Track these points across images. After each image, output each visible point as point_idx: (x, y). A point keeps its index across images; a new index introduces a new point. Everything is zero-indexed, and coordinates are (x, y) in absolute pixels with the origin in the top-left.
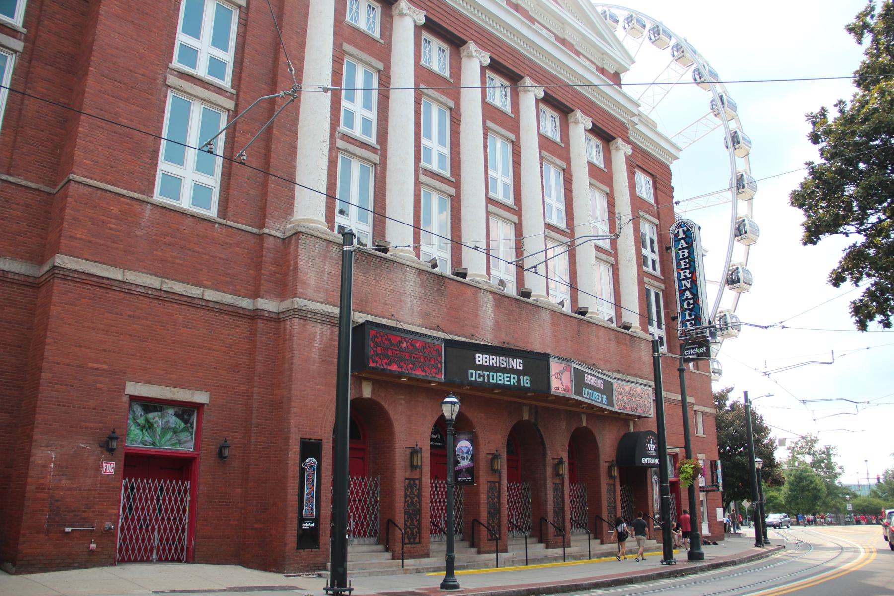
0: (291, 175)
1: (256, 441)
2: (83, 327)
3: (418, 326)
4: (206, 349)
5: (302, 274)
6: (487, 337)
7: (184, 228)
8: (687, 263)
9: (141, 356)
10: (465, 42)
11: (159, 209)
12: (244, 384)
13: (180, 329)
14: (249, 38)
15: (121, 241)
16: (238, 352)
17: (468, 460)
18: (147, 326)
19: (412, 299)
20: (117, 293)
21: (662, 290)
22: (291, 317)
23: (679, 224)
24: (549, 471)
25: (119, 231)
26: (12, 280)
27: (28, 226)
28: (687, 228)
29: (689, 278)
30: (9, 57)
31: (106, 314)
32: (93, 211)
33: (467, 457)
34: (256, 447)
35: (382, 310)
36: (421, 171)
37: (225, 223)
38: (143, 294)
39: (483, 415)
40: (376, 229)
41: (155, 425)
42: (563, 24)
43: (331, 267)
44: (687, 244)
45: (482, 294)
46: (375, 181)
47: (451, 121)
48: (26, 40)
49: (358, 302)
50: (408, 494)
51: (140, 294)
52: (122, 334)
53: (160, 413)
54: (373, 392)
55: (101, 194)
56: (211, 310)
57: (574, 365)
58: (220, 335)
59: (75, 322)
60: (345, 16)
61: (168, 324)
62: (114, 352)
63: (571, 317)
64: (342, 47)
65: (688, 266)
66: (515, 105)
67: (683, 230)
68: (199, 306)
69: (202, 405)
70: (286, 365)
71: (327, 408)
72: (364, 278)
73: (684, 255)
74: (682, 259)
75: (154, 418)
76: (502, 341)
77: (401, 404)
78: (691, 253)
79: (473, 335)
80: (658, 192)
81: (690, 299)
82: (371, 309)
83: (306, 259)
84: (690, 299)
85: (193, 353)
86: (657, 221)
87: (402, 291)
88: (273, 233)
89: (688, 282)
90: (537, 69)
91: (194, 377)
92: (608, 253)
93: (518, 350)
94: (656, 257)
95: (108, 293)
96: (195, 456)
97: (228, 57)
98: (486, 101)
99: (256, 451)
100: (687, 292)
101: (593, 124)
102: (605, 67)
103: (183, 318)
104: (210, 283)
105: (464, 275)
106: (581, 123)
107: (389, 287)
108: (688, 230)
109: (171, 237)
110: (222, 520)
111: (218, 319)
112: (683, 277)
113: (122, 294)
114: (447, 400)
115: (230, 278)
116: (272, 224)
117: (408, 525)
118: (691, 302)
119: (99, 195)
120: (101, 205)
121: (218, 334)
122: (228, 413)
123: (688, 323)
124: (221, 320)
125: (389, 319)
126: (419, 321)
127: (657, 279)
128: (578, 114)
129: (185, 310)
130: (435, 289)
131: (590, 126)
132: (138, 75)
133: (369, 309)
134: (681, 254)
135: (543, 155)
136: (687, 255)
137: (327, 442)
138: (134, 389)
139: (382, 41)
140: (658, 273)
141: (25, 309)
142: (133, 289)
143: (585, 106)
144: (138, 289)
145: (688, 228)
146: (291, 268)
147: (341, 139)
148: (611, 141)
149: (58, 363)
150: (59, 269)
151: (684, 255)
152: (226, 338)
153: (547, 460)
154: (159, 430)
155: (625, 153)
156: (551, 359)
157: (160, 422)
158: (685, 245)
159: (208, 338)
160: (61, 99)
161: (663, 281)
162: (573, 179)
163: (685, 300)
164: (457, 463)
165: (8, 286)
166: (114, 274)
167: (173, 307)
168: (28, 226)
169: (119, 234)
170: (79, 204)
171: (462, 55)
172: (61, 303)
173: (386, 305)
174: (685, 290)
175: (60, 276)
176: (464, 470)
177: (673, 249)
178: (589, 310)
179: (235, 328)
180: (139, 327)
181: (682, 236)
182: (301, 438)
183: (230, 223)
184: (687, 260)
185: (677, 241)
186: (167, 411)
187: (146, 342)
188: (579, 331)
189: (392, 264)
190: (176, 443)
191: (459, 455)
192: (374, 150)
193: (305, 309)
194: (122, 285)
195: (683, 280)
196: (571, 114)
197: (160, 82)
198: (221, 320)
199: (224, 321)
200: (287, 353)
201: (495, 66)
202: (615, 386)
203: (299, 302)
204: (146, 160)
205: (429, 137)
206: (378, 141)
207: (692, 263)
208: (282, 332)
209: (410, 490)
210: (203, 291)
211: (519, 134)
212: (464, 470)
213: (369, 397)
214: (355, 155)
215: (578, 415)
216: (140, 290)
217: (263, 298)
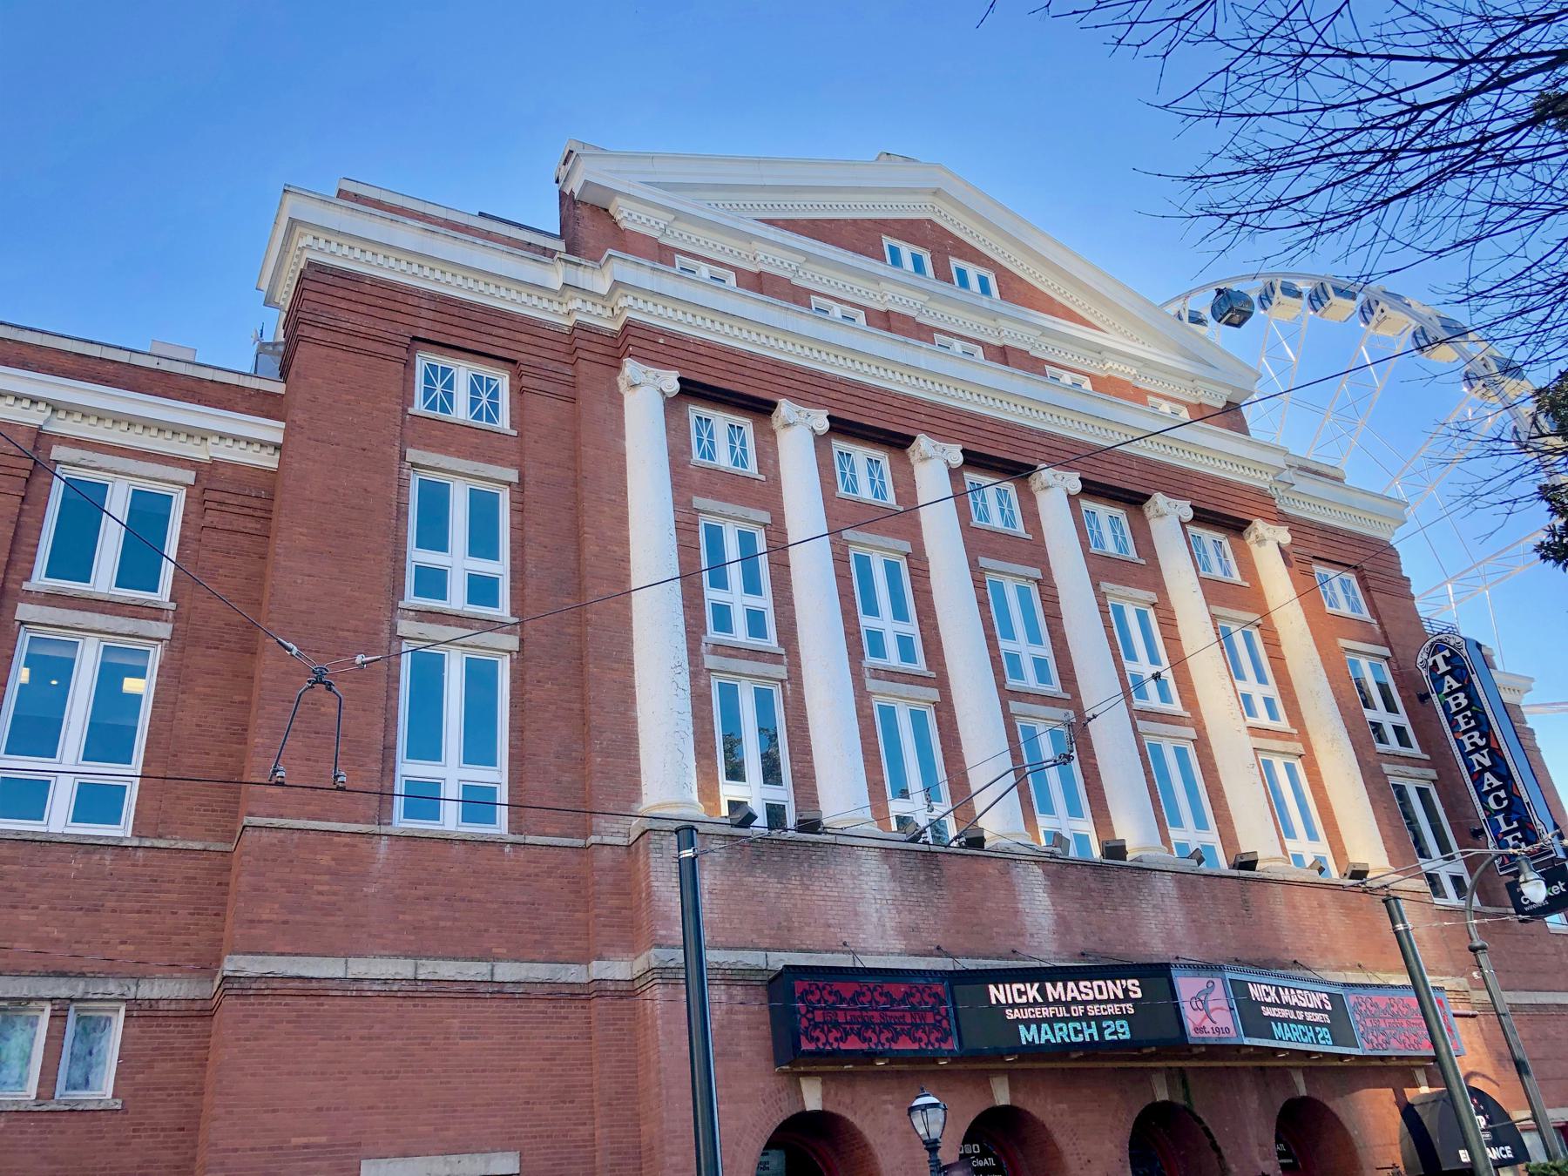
0: (629, 734)
2: (279, 1074)
3: (900, 954)
4: (507, 1070)
5: (661, 904)
7: (449, 865)
8: (1470, 718)
9: (387, 1108)
10: (911, 439)
13: (457, 1044)
14: (531, 531)
15: (340, 910)
16: (567, 1065)
18: (396, 1050)
19: (878, 906)
20: (338, 1001)
22: (649, 985)
23: (1431, 645)
25: (335, 894)
26: (165, 1014)
27: (190, 914)
28: (1451, 651)
29: (1483, 748)
30: (152, 650)
31: (320, 1042)
32: (288, 870)
35: (821, 938)
36: (867, 674)
38: (384, 994)
39: (1065, 1106)
40: (869, 721)
42: (1100, 353)
44: (1458, 681)
49: (773, 932)
52: (350, 1073)
54: (825, 1098)
55: (299, 838)
56: (511, 997)
57: (1229, 975)
59: (264, 1069)
61: (433, 1038)
62: (336, 1109)
64: (692, 505)
65: (1473, 723)
67: (1444, 657)
68: (488, 996)
72: (779, 886)
74: (1457, 713)
77: (887, 1112)
79: (1014, 952)
80: (1375, 595)
81: (1498, 788)
82: (801, 941)
83: (666, 874)
84: (1498, 788)
85: (483, 1082)
86: (1386, 652)
88: (607, 840)
89: (1483, 755)
90: (1058, 445)
91: (489, 1128)
92: (1284, 736)
93: (1117, 966)
94: (1402, 719)
95: (322, 1004)
103: (461, 1022)
107: (829, 894)
109: (428, 884)
112: (1469, 748)
113: (346, 1002)
115: (540, 933)
116: (606, 825)
118: (1502, 794)
119: (296, 841)
120: (301, 856)
123: (1509, 838)
124: (531, 1012)
125: (839, 952)
126: (899, 945)
128: (1159, 499)
129: (462, 1007)
130: (922, 878)
132: (348, 633)
133: (797, 942)
134: (1452, 704)
135: (1103, 589)
136: (1464, 702)
139: (762, 477)
141: (192, 1059)
147: (714, 654)
149: (236, 1150)
150: (232, 980)
152: (543, 1044)
156: (1174, 972)
159: (509, 1049)
160: (235, 697)
163: (1488, 793)
165: (158, 1026)
166: (330, 968)
167: (440, 1006)
168: (190, 914)
169: (334, 898)
170: (262, 863)
171: (912, 461)
172: (238, 1039)
174: (1481, 773)
175: (233, 992)
177: (1434, 696)
180: (380, 1053)
181: (1443, 668)
183: (530, 839)
184: (1468, 713)
185: (1438, 680)
187: (397, 1078)
188: (1245, 901)
189: (829, 850)
192: (775, 658)
195: (1471, 753)
198: (531, 1012)
199: (536, 1012)
200: (651, 1053)
204: (373, 765)
208: (642, 1013)
210: (493, 966)
211: (1048, 564)
215: (1284, 1073)
216: (379, 988)
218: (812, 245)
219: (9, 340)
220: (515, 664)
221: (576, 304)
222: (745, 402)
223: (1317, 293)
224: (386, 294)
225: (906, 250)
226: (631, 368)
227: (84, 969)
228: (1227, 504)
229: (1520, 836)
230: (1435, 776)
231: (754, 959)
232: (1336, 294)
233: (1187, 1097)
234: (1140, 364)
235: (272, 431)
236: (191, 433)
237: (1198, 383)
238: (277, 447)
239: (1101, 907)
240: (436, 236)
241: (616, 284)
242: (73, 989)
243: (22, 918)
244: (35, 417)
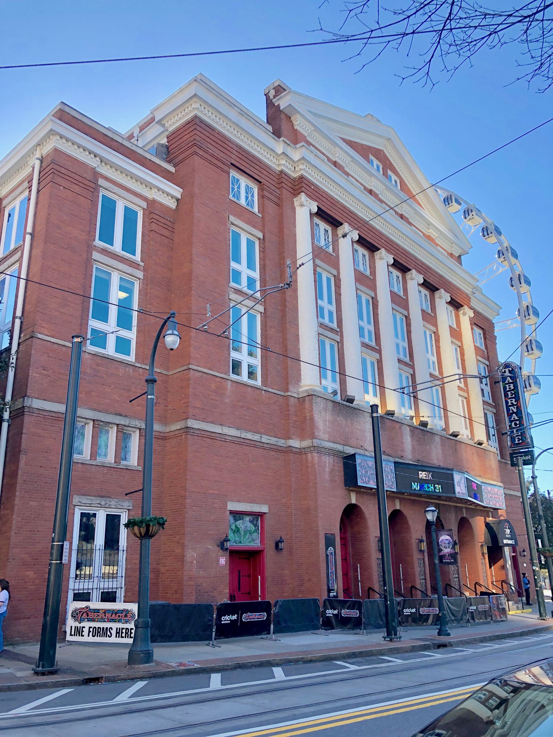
8: (513, 394)
14: (267, 262)
20: (219, 442)
25: (217, 400)
28: (512, 368)
29: (515, 405)
32: (203, 389)
37: (267, 390)
38: (232, 441)
41: (240, 529)
48: (144, 270)
65: (514, 396)
67: (509, 370)
69: (266, 513)
73: (510, 388)
75: (240, 525)
76: (417, 459)
79: (402, 457)
80: (487, 341)
81: (517, 420)
84: (517, 420)
86: (487, 363)
88: (293, 395)
89: (514, 408)
100: (514, 415)
101: (424, 280)
102: (453, 253)
106: (443, 297)
114: (428, 509)
131: (422, 281)
134: (508, 387)
136: (512, 388)
138: (233, 506)
146: (308, 418)
148: (459, 308)
149: (193, 492)
151: (509, 386)
154: (242, 533)
155: (310, 211)
158: (511, 381)
161: (495, 407)
163: (512, 421)
164: (440, 550)
173: (358, 439)
174: (512, 414)
175: (191, 433)
176: (447, 555)
178: (356, 399)
183: (270, 390)
184: (513, 392)
188: (456, 449)
190: (251, 541)
191: (441, 545)
194: (221, 436)
195: (510, 406)
196: (409, 273)
197: (227, 297)
201: (321, 214)
202: (483, 487)
203: (316, 442)
207: (517, 394)
217: (292, 439)
218: (358, 157)
219: (80, 120)
220: (262, 318)
222: (331, 220)
223: (447, 198)
224: (222, 139)
226: (303, 197)
227: (127, 414)
228: (458, 298)
230: (495, 412)
231: (340, 447)
232: (455, 202)
234: (439, 233)
235: (177, 192)
236: (142, 182)
237: (454, 245)
238: (178, 200)
240: (243, 117)
241: (303, 158)
242: (126, 421)
243: (107, 390)
244: (93, 162)
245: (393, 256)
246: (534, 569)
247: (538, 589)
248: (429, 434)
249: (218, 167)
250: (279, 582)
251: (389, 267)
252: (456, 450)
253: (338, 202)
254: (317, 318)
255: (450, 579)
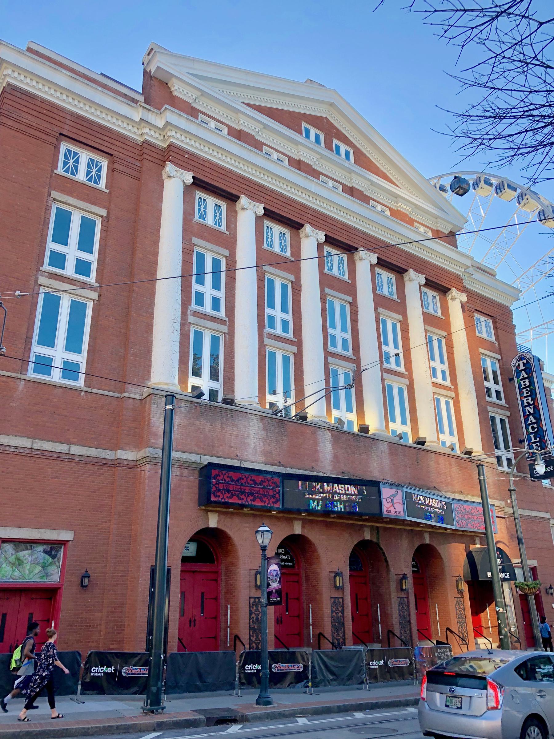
1: (114, 570)
3: (262, 463)
6: (327, 470)
8: (529, 391)
11: (32, 384)
12: (106, 522)
17: (277, 582)
21: (508, 417)
22: (144, 464)
23: (519, 357)
24: (393, 586)
29: (531, 405)
33: (276, 579)
34: (114, 576)
39: (324, 537)
41: (25, 562)
43: (181, 420)
45: (320, 433)
46: (225, 346)
47: (292, 292)
50: (253, 611)
51: (13, 453)
53: (30, 551)
54: (219, 522)
56: (78, 462)
57: (405, 490)
58: (85, 483)
60: (194, 215)
63: (414, 448)
64: (191, 241)
65: (529, 393)
66: (352, 272)
67: (523, 363)
68: (66, 460)
69: (69, 541)
70: (140, 504)
71: (176, 538)
72: (211, 427)
74: (524, 388)
76: (341, 471)
78: (532, 383)
79: (313, 468)
81: (534, 423)
84: (534, 423)
87: (246, 435)
88: (132, 396)
89: (531, 408)
90: (370, 239)
92: (447, 388)
94: (500, 388)
96: (59, 586)
97: (93, 258)
98: (324, 272)
99: (115, 579)
100: (531, 417)
104: (76, 440)
105: (423, 443)
108: (527, 362)
109: (42, 405)
110: (81, 642)
111: (84, 469)
112: (526, 404)
116: (132, 389)
117: (254, 639)
118: (535, 426)
121: (84, 481)
122: (91, 547)
126: (262, 459)
127: (501, 407)
128: (412, 273)
133: (215, 452)
134: (523, 384)
136: (528, 384)
137: (175, 568)
140: (503, 402)
142: (7, 449)
143: (419, 266)
144: (12, 450)
145: (527, 361)
146: (146, 423)
153: (391, 576)
157: (30, 559)
158: (526, 376)
162: (410, 328)
163: (530, 424)
173: (231, 447)
174: (528, 415)
176: (274, 591)
177: (516, 380)
178: (427, 440)
179: (98, 476)
182: (151, 566)
183: (94, 391)
186: (36, 549)
188: (418, 459)
190: (43, 576)
192: (223, 322)
193: (156, 456)
195: (526, 406)
196: (406, 274)
197: (32, 282)
198: (86, 470)
201: (429, 284)
205: (333, 326)
206: (226, 315)
207: (533, 391)
208: (139, 476)
209: (255, 608)
212: (274, 591)
213: (216, 527)
214: (441, 394)
215: (420, 534)
217: (122, 449)
218: (272, 123)
221: (146, 130)
225: (313, 131)
226: (170, 168)
228: (442, 280)
229: (539, 445)
231: (195, 458)
233: (378, 538)
234: (413, 207)
239: (354, 453)
245: (425, 276)
246: (497, 610)
247: (502, 637)
248: (423, 453)
249: (39, 139)
250: (82, 629)
251: (422, 288)
252: (417, 460)
253: (231, 171)
254: (431, 379)
255: (392, 624)
